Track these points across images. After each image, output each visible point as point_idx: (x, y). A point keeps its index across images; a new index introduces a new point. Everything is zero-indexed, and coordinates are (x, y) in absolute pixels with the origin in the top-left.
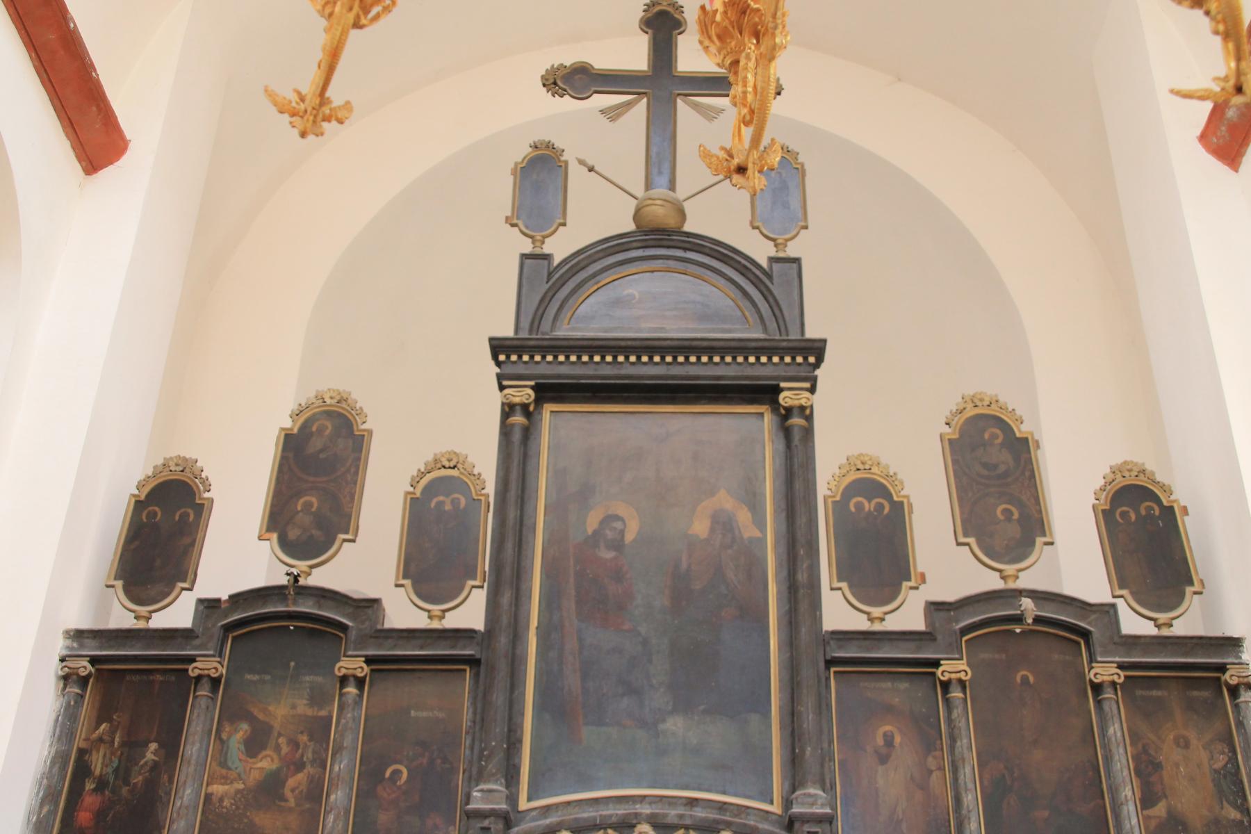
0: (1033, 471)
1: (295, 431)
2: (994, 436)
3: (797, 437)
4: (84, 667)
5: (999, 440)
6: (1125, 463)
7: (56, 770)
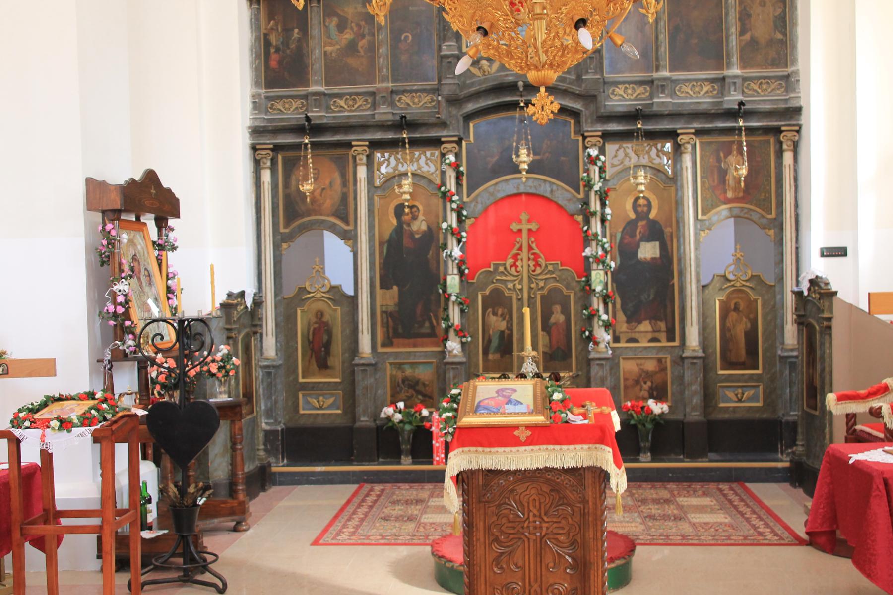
7: (257, 44)
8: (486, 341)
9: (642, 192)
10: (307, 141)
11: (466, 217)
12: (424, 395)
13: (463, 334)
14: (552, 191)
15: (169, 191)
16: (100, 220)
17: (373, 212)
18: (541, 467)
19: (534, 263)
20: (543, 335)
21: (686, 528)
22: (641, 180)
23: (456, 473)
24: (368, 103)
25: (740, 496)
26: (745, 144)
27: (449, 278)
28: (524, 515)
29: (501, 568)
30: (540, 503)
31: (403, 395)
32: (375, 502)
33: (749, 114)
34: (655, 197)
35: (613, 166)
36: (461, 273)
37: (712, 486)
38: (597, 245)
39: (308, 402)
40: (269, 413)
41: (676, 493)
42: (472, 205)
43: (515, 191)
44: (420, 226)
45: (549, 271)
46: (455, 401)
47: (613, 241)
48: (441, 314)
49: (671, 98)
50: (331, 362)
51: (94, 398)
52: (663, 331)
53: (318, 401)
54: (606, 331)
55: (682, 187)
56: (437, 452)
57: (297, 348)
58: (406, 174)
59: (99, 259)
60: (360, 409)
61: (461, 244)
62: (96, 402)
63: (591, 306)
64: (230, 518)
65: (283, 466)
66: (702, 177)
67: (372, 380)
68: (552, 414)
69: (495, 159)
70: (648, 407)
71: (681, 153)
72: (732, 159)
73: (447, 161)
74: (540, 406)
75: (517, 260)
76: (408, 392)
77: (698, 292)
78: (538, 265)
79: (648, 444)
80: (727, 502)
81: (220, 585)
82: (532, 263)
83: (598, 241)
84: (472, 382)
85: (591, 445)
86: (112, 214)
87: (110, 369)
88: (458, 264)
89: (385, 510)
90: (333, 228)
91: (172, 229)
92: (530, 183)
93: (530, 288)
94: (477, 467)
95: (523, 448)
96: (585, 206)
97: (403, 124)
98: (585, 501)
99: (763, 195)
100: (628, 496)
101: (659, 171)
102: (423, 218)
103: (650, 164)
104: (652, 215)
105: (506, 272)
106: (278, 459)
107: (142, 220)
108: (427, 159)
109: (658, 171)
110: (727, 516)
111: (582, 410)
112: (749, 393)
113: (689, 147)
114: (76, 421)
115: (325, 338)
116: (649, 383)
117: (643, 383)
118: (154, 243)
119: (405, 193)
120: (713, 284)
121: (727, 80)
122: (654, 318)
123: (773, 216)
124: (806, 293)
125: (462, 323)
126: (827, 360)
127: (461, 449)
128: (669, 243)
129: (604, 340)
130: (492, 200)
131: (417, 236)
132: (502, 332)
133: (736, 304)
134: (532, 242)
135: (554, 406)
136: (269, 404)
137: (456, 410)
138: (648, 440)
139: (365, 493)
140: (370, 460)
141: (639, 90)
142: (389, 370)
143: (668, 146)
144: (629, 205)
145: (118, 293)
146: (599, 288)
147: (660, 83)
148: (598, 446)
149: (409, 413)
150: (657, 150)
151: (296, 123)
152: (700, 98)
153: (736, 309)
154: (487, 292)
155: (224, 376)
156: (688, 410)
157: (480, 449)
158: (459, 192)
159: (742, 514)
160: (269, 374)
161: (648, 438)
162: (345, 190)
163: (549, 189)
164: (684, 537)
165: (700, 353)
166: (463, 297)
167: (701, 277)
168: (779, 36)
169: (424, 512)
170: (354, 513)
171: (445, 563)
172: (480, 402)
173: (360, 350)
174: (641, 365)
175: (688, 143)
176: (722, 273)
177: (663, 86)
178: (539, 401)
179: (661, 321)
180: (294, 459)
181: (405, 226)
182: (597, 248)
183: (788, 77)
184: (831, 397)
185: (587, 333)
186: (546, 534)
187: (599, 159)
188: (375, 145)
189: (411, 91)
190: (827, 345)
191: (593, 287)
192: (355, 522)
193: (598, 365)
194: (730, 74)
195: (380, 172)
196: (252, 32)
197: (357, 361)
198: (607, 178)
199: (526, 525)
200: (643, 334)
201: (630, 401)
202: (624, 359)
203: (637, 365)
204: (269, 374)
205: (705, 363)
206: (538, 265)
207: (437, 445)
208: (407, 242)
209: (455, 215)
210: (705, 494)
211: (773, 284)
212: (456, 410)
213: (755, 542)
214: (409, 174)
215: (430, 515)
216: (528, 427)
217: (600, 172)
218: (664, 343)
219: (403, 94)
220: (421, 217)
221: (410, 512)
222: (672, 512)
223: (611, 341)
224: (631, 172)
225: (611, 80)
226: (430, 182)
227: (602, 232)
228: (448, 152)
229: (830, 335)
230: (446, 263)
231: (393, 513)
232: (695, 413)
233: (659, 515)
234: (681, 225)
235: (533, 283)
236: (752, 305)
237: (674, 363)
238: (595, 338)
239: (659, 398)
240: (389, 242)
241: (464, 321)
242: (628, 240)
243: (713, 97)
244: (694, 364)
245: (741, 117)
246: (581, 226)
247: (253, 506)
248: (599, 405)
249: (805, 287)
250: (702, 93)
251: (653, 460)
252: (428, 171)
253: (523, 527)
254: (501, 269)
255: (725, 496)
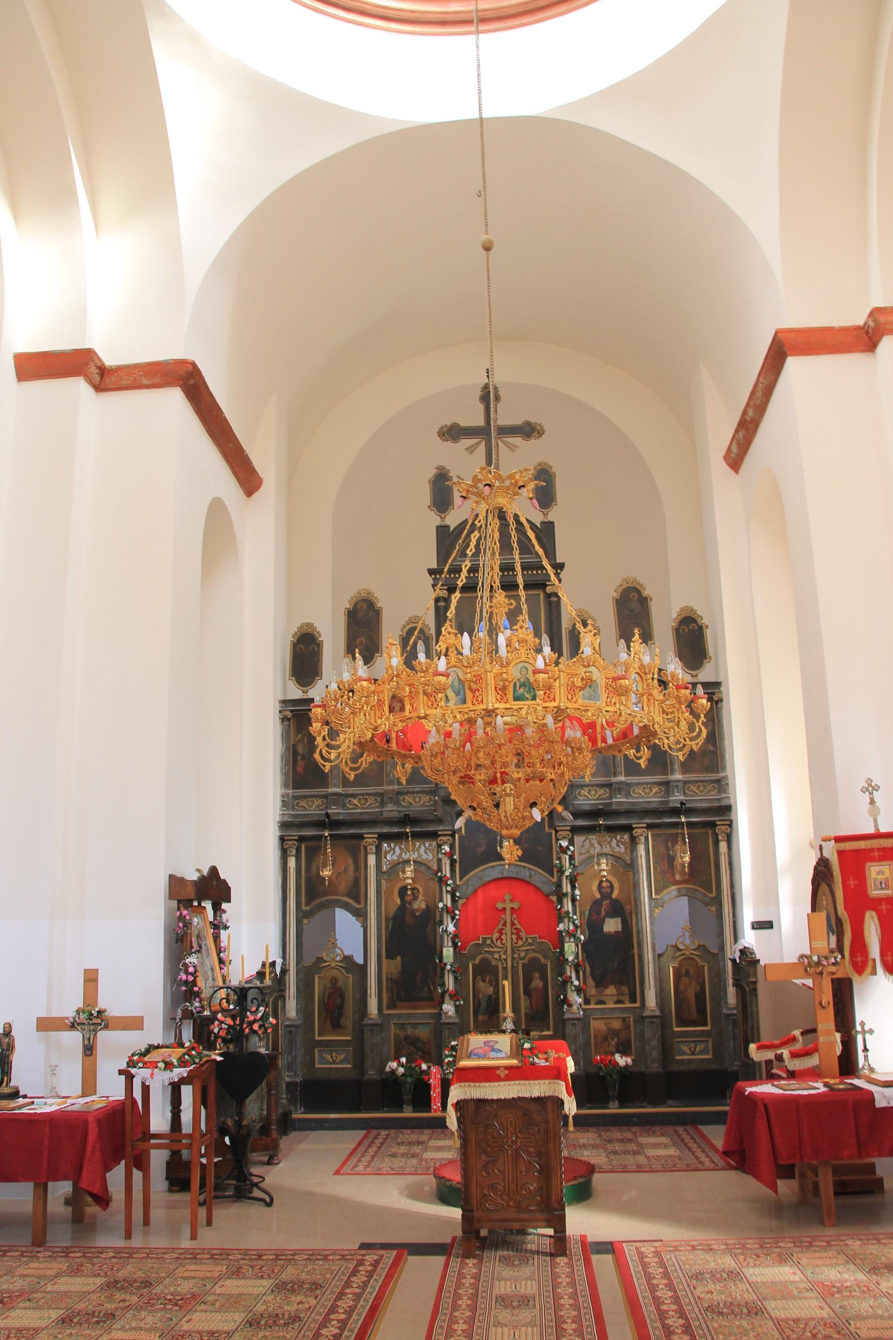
2: (634, 597)
3: (553, 606)
4: (289, 714)
8: (476, 1005)
9: (605, 876)
11: (458, 897)
12: (423, 1052)
14: (530, 876)
15: (224, 882)
16: (176, 906)
17: (381, 893)
20: (524, 999)
21: (641, 1159)
22: (604, 866)
23: (455, 1101)
24: (377, 802)
27: (445, 950)
30: (515, 1124)
32: (382, 1143)
33: (689, 812)
34: (616, 880)
35: (581, 854)
36: (455, 945)
37: (670, 1129)
38: (569, 921)
39: (323, 1057)
40: (290, 1067)
43: (500, 876)
44: (420, 904)
48: (438, 981)
55: (638, 871)
56: (435, 1101)
57: (314, 1009)
58: (407, 862)
59: (175, 937)
60: (368, 1064)
64: (265, 1153)
66: (654, 863)
67: (379, 1038)
69: (483, 848)
71: (637, 844)
74: (514, 1052)
77: (654, 960)
78: (519, 938)
79: (616, 1094)
81: (268, 1200)
82: (514, 937)
83: (570, 918)
84: (466, 1036)
86: (185, 903)
87: (180, 1026)
88: (452, 938)
90: (346, 907)
91: (225, 912)
93: (513, 958)
94: (470, 1098)
97: (406, 820)
98: (546, 1122)
101: (619, 858)
104: (614, 896)
107: (203, 905)
109: (617, 858)
111: (545, 1056)
113: (643, 839)
114: (176, 1063)
115: (339, 1001)
119: (408, 878)
120: (667, 953)
122: (618, 983)
123: (714, 895)
124: (738, 961)
126: (755, 1016)
127: (458, 1084)
128: (629, 919)
130: (481, 883)
131: (417, 914)
132: (490, 996)
133: (686, 970)
135: (524, 1053)
136: (290, 1059)
137: (455, 1056)
141: (601, 791)
142: (393, 1030)
143: (626, 836)
144: (595, 887)
146: (571, 958)
148: (555, 1081)
152: (650, 798)
153: (687, 974)
154: (477, 962)
155: (263, 1033)
156: (649, 1062)
157: (472, 1084)
158: (453, 877)
159: (689, 1149)
160: (291, 1032)
162: (357, 875)
163: (528, 874)
164: (638, 1166)
165: (658, 1013)
166: (456, 966)
168: (711, 748)
169: (425, 1150)
170: (366, 1151)
173: (369, 1012)
174: (609, 1023)
175: (642, 835)
176: (674, 944)
179: (624, 985)
180: (310, 1108)
183: (718, 781)
185: (562, 997)
187: (569, 849)
188: (383, 837)
189: (413, 793)
190: (754, 1004)
191: (566, 957)
192: (367, 1158)
193: (572, 1024)
196: (283, 743)
197: (366, 1021)
198: (576, 864)
200: (610, 997)
203: (605, 1024)
205: (663, 1020)
206: (519, 938)
208: (408, 919)
209: (449, 897)
210: (662, 1135)
211: (716, 952)
212: (455, 1056)
215: (430, 1153)
217: (570, 860)
218: (628, 1005)
220: (421, 898)
222: (632, 1149)
223: (582, 1004)
226: (428, 867)
227: (573, 910)
229: (756, 996)
230: (442, 937)
231: (399, 1151)
233: (622, 1151)
234: (638, 903)
237: (636, 1021)
239: (625, 1053)
241: (457, 986)
243: (662, 797)
244: (652, 1022)
245: (683, 814)
246: (555, 905)
248: (557, 1052)
249: (737, 955)
250: (651, 794)
252: (427, 859)
253: (503, 1142)
254: (489, 942)
255: (679, 1136)
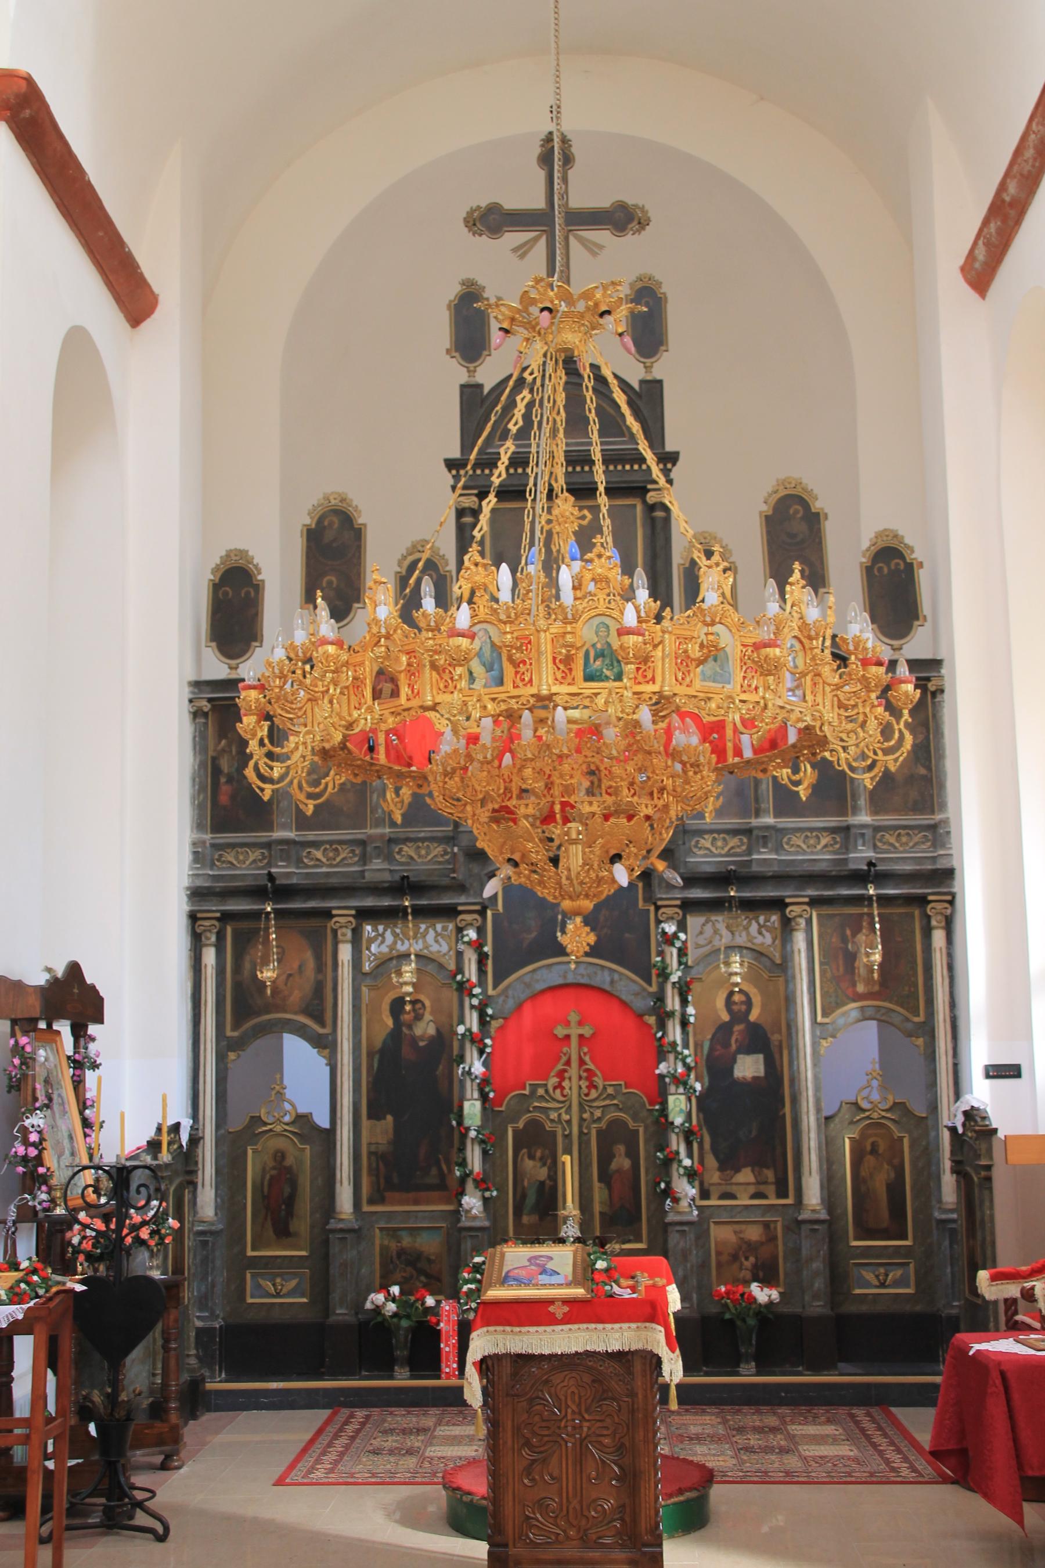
0: (821, 538)
1: (313, 526)
2: (796, 512)
3: (659, 525)
4: (206, 706)
5: (799, 515)
6: (885, 530)
7: (202, 772)
9: (737, 984)
10: (269, 909)
11: (491, 1017)
12: (428, 1276)
13: (485, 1186)
14: (612, 982)
15: (93, 988)
16: (8, 1030)
18: (580, 1350)
19: (587, 1083)
21: (792, 1462)
22: (736, 968)
23: (479, 1357)
24: (355, 855)
25: (878, 1424)
26: (877, 919)
27: (467, 1105)
28: (560, 1411)
29: (533, 1480)
30: (580, 1397)
31: (398, 1275)
32: (358, 1431)
33: (881, 878)
35: (698, 946)
36: (484, 1097)
37: (842, 1411)
38: (676, 1058)
39: (260, 1286)
40: (203, 1302)
41: (788, 1419)
42: (501, 1000)
43: (561, 981)
44: (426, 1028)
45: (609, 1095)
46: (478, 1272)
47: (699, 1054)
48: (455, 1157)
49: (777, 853)
50: (295, 1225)
51: (17, 1269)
52: (771, 1183)
53: (274, 1285)
54: (689, 1182)
55: (794, 977)
56: (448, 1360)
57: (245, 1205)
60: (335, 1296)
61: (484, 1056)
62: (21, 1274)
63: (668, 1146)
64: (158, 1449)
65: (220, 1382)
66: (821, 964)
67: (355, 1252)
68: (594, 1286)
69: (534, 935)
70: (750, 1294)
71: (792, 930)
72: (861, 938)
73: (466, 939)
75: (562, 1079)
76: (405, 1271)
77: (819, 1126)
78: (592, 1086)
79: (752, 1350)
80: (857, 1431)
81: (160, 1530)
82: (584, 1084)
83: (677, 1054)
84: (499, 1248)
85: (639, 1324)
87: (13, 1233)
88: (479, 1084)
89: (373, 1441)
90: (301, 1031)
91: (93, 1039)
92: (582, 970)
93: (582, 1120)
94: (504, 1352)
95: (560, 1327)
96: (659, 1003)
97: (404, 886)
98: (632, 1394)
99: (907, 988)
100: (719, 1423)
101: (761, 954)
102: (431, 1018)
103: (749, 945)
104: (753, 1016)
105: (548, 1097)
106: (213, 1371)
108: (437, 934)
110: (853, 1448)
111: (631, 1282)
112: (895, 1274)
113: (802, 922)
115: (287, 1190)
116: (752, 1259)
117: (743, 1259)
118: (69, 1058)
119: (406, 983)
120: (840, 1115)
121: (853, 831)
122: (758, 1164)
123: (921, 1019)
124: (960, 1130)
125: (484, 1170)
127: (485, 1329)
128: (777, 1056)
129: (686, 1195)
130: (528, 993)
131: (421, 1044)
132: (542, 1184)
133: (873, 1144)
134: (585, 1054)
135: (596, 1276)
136: (203, 1288)
138: (751, 1344)
139: (343, 1420)
140: (348, 1374)
141: (734, 841)
142: (378, 1239)
143: (775, 918)
144: (720, 1003)
145: (31, 1129)
146: (678, 1121)
147: (761, 834)
148: (647, 1324)
149: (406, 1302)
150: (759, 924)
151: (253, 883)
152: (817, 853)
153: (874, 1151)
154: (521, 1125)
155: (157, 1245)
156: (807, 1298)
157: (508, 1329)
159: (874, 1446)
161: (750, 1340)
162: (320, 977)
163: (608, 979)
164: (788, 1473)
165: (823, 1215)
166: (486, 1132)
167: (823, 1104)
168: (923, 771)
169: (429, 1443)
170: (330, 1445)
171: (461, 1496)
172: (508, 1272)
173: (338, 1209)
174: (741, 1232)
175: (801, 916)
176: (852, 1099)
177: (765, 837)
178: (579, 1270)
179: (768, 1168)
181: (405, 1030)
182: (675, 1064)
183: (933, 828)
184: (983, 1275)
185: (663, 1185)
186: (588, 1436)
187: (678, 938)
188: (364, 915)
190: (987, 1204)
191: (670, 1119)
192: (332, 1456)
194: (856, 822)
195: (370, 951)
197: (333, 1224)
198: (690, 963)
199: (563, 1424)
200: (741, 1188)
201: (725, 1285)
202: (715, 1223)
203: (735, 1232)
204: (205, 1243)
206: (592, 1086)
207: (447, 1349)
208: (407, 1052)
209: (475, 1015)
210: (829, 1421)
212: (480, 1282)
213: (884, 1479)
214: (413, 957)
215: (437, 1448)
216: (566, 1302)
219: (404, 844)
220: (428, 1017)
221: (409, 1444)
222: (778, 1443)
223: (697, 1197)
224: (722, 957)
225: (694, 828)
226: (441, 966)
227: (683, 1040)
228: (467, 925)
229: (991, 1189)
230: (462, 1083)
232: (818, 1303)
234: (793, 1030)
235: (585, 1112)
236: (896, 1144)
237: (787, 1229)
238: (675, 1192)
239: (767, 1282)
240: (382, 1052)
241: (487, 1166)
242: (719, 1051)
243: (835, 853)
245: (872, 882)
246: (654, 1031)
247: (191, 1431)
248: (651, 1277)
250: (819, 847)
251: (758, 1374)
252: (439, 952)
253: (559, 1428)
254: (541, 1091)
255: (857, 1423)
